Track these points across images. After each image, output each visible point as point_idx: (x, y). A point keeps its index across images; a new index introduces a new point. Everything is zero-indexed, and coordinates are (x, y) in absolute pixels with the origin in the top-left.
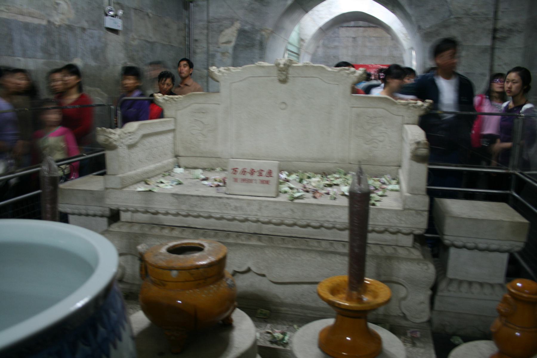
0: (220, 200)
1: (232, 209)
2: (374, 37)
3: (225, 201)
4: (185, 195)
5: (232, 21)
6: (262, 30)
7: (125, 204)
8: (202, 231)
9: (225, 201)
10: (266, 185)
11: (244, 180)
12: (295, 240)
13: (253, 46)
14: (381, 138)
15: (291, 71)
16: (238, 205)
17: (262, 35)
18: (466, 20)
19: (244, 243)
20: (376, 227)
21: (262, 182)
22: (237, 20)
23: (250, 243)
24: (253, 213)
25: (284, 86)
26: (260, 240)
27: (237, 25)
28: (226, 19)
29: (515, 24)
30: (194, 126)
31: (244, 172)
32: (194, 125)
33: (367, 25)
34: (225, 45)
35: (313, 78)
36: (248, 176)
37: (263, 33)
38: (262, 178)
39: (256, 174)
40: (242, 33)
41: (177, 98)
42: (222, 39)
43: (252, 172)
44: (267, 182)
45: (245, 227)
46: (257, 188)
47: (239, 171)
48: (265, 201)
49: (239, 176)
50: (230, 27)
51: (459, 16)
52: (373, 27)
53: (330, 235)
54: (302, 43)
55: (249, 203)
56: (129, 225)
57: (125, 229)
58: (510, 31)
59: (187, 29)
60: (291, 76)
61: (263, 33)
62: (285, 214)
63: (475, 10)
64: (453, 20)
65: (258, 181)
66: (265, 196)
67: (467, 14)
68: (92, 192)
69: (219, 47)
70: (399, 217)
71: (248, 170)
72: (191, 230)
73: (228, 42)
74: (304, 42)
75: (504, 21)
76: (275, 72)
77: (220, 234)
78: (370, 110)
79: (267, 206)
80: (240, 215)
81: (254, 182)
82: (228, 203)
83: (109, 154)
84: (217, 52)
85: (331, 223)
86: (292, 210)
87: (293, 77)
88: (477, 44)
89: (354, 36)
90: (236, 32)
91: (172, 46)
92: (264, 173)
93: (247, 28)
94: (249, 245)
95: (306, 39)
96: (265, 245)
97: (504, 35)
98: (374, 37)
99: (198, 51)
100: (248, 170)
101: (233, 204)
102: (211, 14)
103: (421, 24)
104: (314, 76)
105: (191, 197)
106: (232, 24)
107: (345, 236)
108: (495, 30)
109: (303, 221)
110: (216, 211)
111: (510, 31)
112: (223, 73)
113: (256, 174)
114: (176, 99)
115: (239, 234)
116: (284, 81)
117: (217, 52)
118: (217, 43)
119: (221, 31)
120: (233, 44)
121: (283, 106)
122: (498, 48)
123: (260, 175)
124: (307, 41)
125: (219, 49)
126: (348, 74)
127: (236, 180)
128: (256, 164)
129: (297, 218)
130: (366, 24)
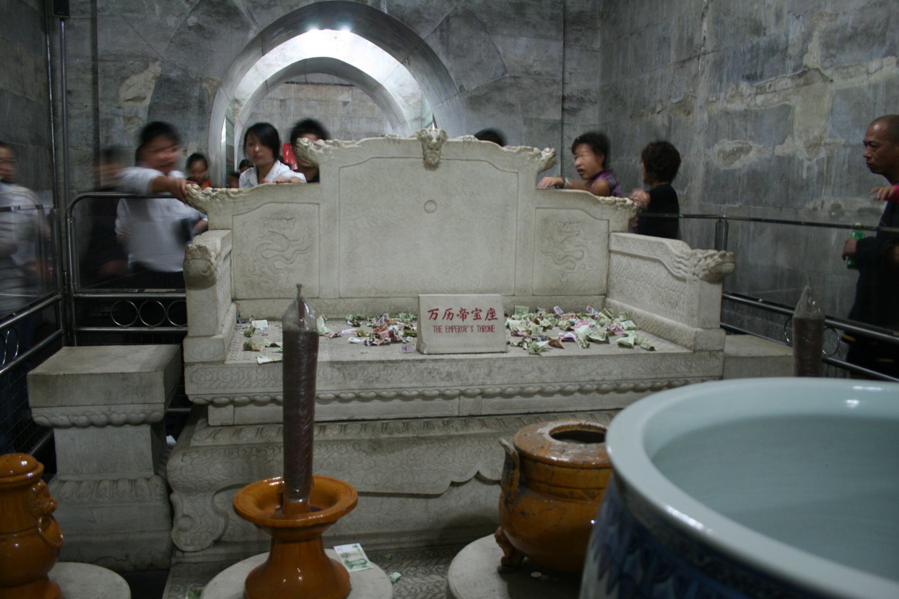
0: (422, 366)
1: (442, 379)
2: (315, 100)
3: (431, 365)
4: (356, 363)
5: (146, 62)
6: (201, 80)
7: (228, 391)
8: (379, 423)
9: (431, 365)
10: (490, 333)
11: (452, 328)
12: (538, 418)
13: (186, 107)
14: (579, 255)
15: (444, 150)
16: (453, 370)
17: (201, 89)
18: (526, 82)
19: (461, 433)
20: (528, 387)
21: (482, 329)
22: (156, 60)
23: (471, 432)
24: (475, 381)
25: (431, 174)
26: (484, 425)
27: (156, 69)
28: (131, 56)
29: (587, 92)
30: (269, 244)
31: (449, 315)
32: (269, 241)
33: (339, 83)
34: (131, 103)
35: (478, 162)
36: (457, 321)
37: (205, 85)
38: (479, 322)
39: (470, 317)
40: (163, 82)
41: (233, 193)
42: (127, 92)
43: (463, 314)
44: (491, 329)
45: (452, 408)
46: (475, 340)
47: (441, 313)
48: (498, 359)
49: (441, 321)
50: (141, 72)
51: (517, 75)
52: (347, 85)
53: (251, 413)
54: (237, 106)
55: (472, 365)
56: (231, 430)
57: (224, 439)
58: (581, 101)
59: (49, 71)
60: (444, 158)
61: (205, 85)
62: (529, 377)
63: (537, 68)
64: (508, 81)
65: (475, 328)
66: (491, 351)
67: (528, 73)
68: (124, 376)
69: (119, 108)
70: (689, 364)
71: (456, 311)
72: (358, 424)
73: (138, 99)
74: (241, 106)
75: (574, 86)
76: (418, 152)
77: (414, 423)
78: (563, 212)
79: (500, 367)
80: (453, 387)
81: (469, 329)
82: (434, 369)
83: (194, 298)
84: (118, 115)
85: (437, 388)
86: (540, 370)
87: (448, 159)
88: (543, 117)
89: (282, 98)
90: (154, 81)
91: (28, 100)
92: (483, 315)
93: (173, 75)
94: (470, 436)
95: (244, 100)
96: (494, 431)
97: (575, 106)
98: (315, 100)
99: (74, 112)
100: (456, 311)
101: (445, 368)
102: (101, 46)
103: (464, 83)
104: (480, 158)
105: (368, 365)
106: (146, 67)
107: (276, 412)
108: (564, 99)
109: (555, 385)
110: (414, 384)
111: (581, 101)
112: (326, 150)
113: (470, 317)
114: (232, 195)
115: (446, 420)
116: (431, 166)
117: (118, 115)
118: (115, 99)
119: (124, 78)
120: (147, 102)
121: (430, 207)
122: (566, 124)
123: (477, 317)
124: (245, 103)
125: (121, 112)
126: (534, 157)
127: (438, 329)
128: (469, 301)
129: (549, 380)
130: (336, 80)
